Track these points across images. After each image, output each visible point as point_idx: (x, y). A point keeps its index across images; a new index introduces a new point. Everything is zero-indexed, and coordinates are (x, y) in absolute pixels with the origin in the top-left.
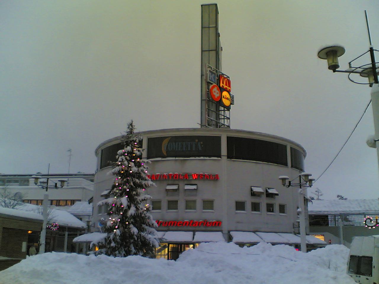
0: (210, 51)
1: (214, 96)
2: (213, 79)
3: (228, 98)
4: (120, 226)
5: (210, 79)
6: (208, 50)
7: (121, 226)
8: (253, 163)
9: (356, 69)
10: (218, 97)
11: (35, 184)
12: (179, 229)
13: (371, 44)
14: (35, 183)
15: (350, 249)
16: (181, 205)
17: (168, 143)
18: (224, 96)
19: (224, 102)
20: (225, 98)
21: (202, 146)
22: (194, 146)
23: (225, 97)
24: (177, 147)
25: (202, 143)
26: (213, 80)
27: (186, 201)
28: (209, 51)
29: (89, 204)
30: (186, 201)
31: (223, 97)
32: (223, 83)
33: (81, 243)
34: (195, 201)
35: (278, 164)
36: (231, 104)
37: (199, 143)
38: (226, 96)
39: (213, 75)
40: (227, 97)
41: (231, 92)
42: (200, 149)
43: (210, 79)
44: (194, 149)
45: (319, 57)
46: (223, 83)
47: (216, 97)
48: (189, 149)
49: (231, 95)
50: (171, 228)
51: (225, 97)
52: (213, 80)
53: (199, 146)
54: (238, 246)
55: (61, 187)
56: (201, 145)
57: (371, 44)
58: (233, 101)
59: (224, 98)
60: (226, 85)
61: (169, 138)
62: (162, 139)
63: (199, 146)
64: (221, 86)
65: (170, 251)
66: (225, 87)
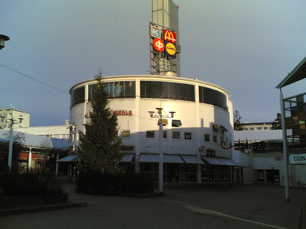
0: (158, 11)
1: (157, 47)
2: (157, 34)
3: (172, 48)
4: (7, 135)
5: (154, 34)
6: (157, 10)
7: (7, 136)
8: (210, 107)
9: (182, 155)
10: (161, 48)
11: (151, 117)
14: (151, 116)
18: (168, 47)
19: (168, 52)
20: (169, 49)
23: (169, 48)
26: (157, 35)
28: (158, 10)
29: (202, 118)
31: (167, 48)
32: (167, 36)
35: (220, 107)
36: (177, 53)
38: (170, 47)
39: (157, 31)
40: (171, 48)
43: (154, 34)
45: (217, 125)
46: (167, 36)
47: (159, 49)
49: (176, 45)
51: (169, 48)
52: (157, 35)
55: (172, 117)
58: (180, 50)
59: (168, 48)
60: (171, 37)
64: (165, 39)
65: (36, 152)
66: (170, 39)
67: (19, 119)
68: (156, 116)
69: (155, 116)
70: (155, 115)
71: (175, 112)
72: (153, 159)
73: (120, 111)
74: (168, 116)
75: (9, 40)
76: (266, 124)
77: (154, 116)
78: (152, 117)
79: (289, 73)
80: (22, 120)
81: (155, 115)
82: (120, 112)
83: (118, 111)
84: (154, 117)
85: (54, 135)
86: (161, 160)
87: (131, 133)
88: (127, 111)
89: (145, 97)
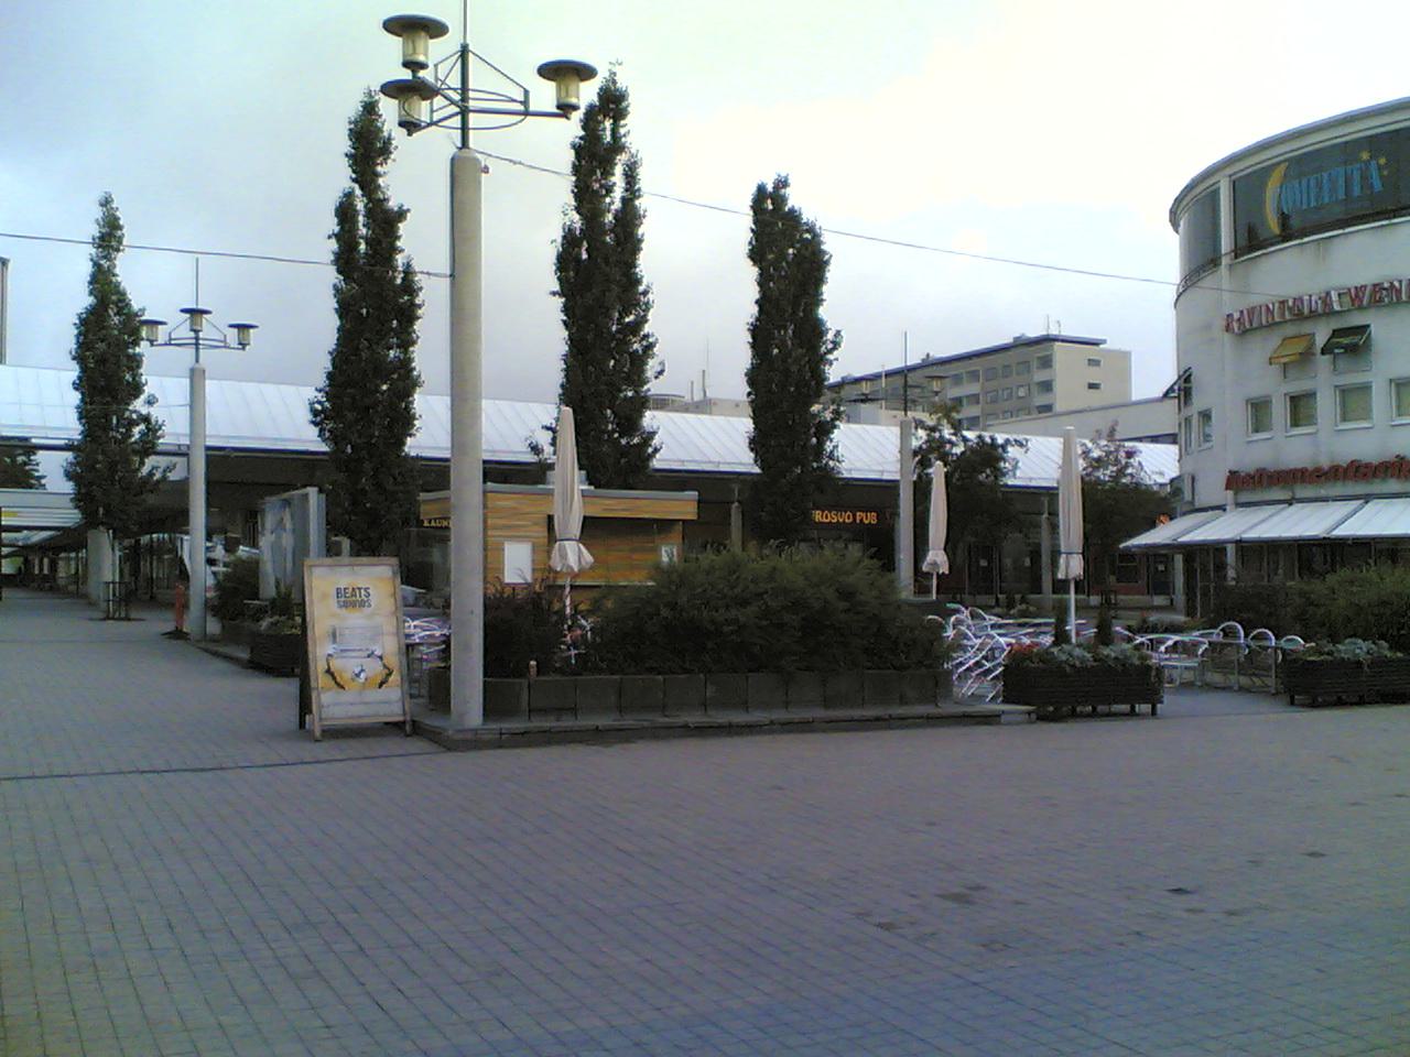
12: (1323, 492)
13: (197, 361)
15: (1177, 447)
16: (1326, 404)
17: (1281, 187)
21: (1385, 173)
22: (1357, 176)
24: (1305, 200)
25: (1382, 161)
27: (1292, 398)
30: (1292, 398)
33: (1159, 555)
34: (1366, 388)
37: (1373, 162)
41: (144, 366)
42: (1378, 185)
44: (1357, 191)
48: (1342, 196)
50: (1301, 492)
53: (1375, 174)
54: (84, 300)
56: (1380, 168)
57: (197, 361)
61: (1283, 166)
62: (1263, 174)
63: (1375, 174)
67: (236, 330)
68: (173, 342)
69: (170, 339)
70: (170, 334)
71: (164, 320)
72: (354, 559)
73: (1375, 285)
74: (225, 341)
75: (446, 37)
76: (31, 438)
77: (162, 339)
78: (152, 345)
79: (557, 288)
80: (251, 331)
81: (170, 334)
82: (1377, 287)
83: (1365, 287)
84: (166, 344)
85: (447, 641)
86: (345, 559)
87: (637, 202)
88: (1328, 294)
89: (886, 375)
